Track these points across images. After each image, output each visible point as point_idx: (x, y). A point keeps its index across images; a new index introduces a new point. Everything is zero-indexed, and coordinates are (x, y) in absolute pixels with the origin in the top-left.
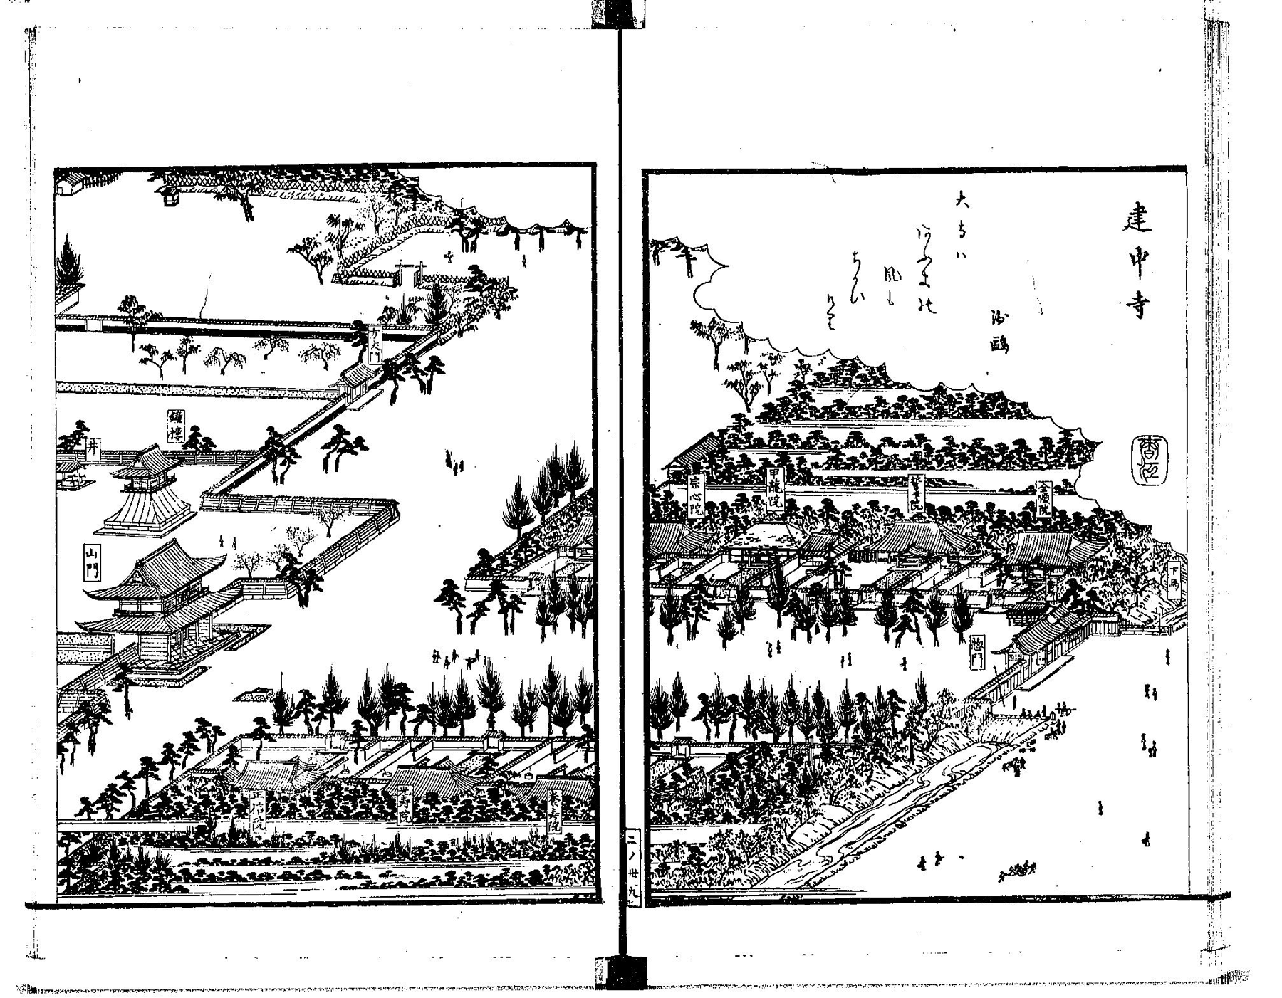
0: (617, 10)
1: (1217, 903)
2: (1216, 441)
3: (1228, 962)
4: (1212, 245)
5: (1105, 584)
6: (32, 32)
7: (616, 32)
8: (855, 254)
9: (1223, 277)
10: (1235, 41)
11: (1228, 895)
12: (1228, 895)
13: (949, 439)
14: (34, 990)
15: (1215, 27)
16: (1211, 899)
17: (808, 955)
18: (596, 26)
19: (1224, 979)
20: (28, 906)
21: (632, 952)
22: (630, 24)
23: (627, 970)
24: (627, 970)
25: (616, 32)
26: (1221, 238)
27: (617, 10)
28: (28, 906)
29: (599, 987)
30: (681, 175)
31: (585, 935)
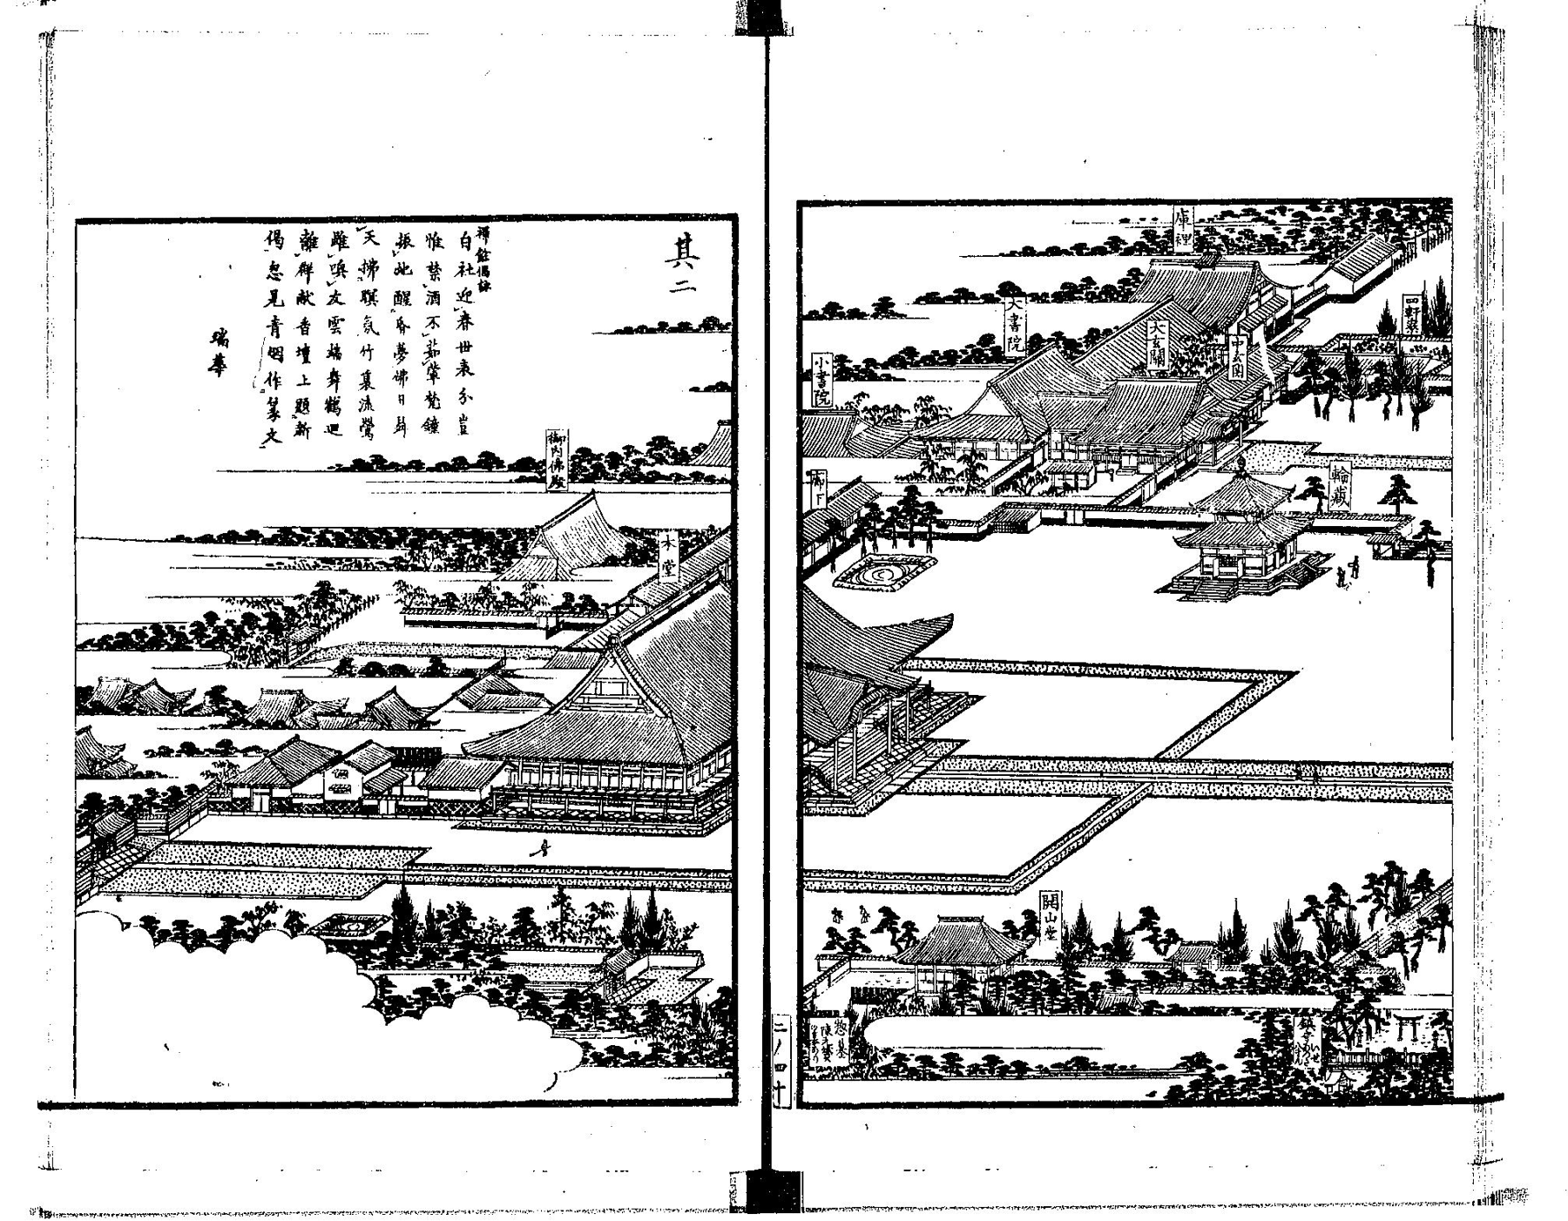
0: (763, 12)
1: (1487, 1105)
2: (1487, 543)
3: (1497, 1179)
4: (1483, 302)
5: (421, 721)
6: (49, 37)
7: (763, 39)
8: (219, 364)
9: (1496, 341)
10: (1513, 55)
11: (1500, 1097)
12: (1500, 1097)
13: (912, 545)
14: (49, 1215)
15: (1484, 34)
16: (1478, 1101)
17: (993, 1170)
18: (739, 32)
19: (1494, 1199)
20: (42, 1106)
21: (779, 1164)
22: (780, 31)
23: (773, 1188)
24: (773, 1188)
25: (763, 39)
26: (1494, 293)
27: (763, 12)
28: (42, 1106)
29: (733, 1210)
30: (990, 198)
31: (730, 1143)
